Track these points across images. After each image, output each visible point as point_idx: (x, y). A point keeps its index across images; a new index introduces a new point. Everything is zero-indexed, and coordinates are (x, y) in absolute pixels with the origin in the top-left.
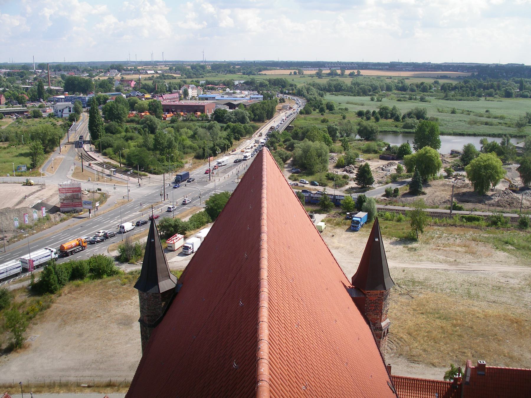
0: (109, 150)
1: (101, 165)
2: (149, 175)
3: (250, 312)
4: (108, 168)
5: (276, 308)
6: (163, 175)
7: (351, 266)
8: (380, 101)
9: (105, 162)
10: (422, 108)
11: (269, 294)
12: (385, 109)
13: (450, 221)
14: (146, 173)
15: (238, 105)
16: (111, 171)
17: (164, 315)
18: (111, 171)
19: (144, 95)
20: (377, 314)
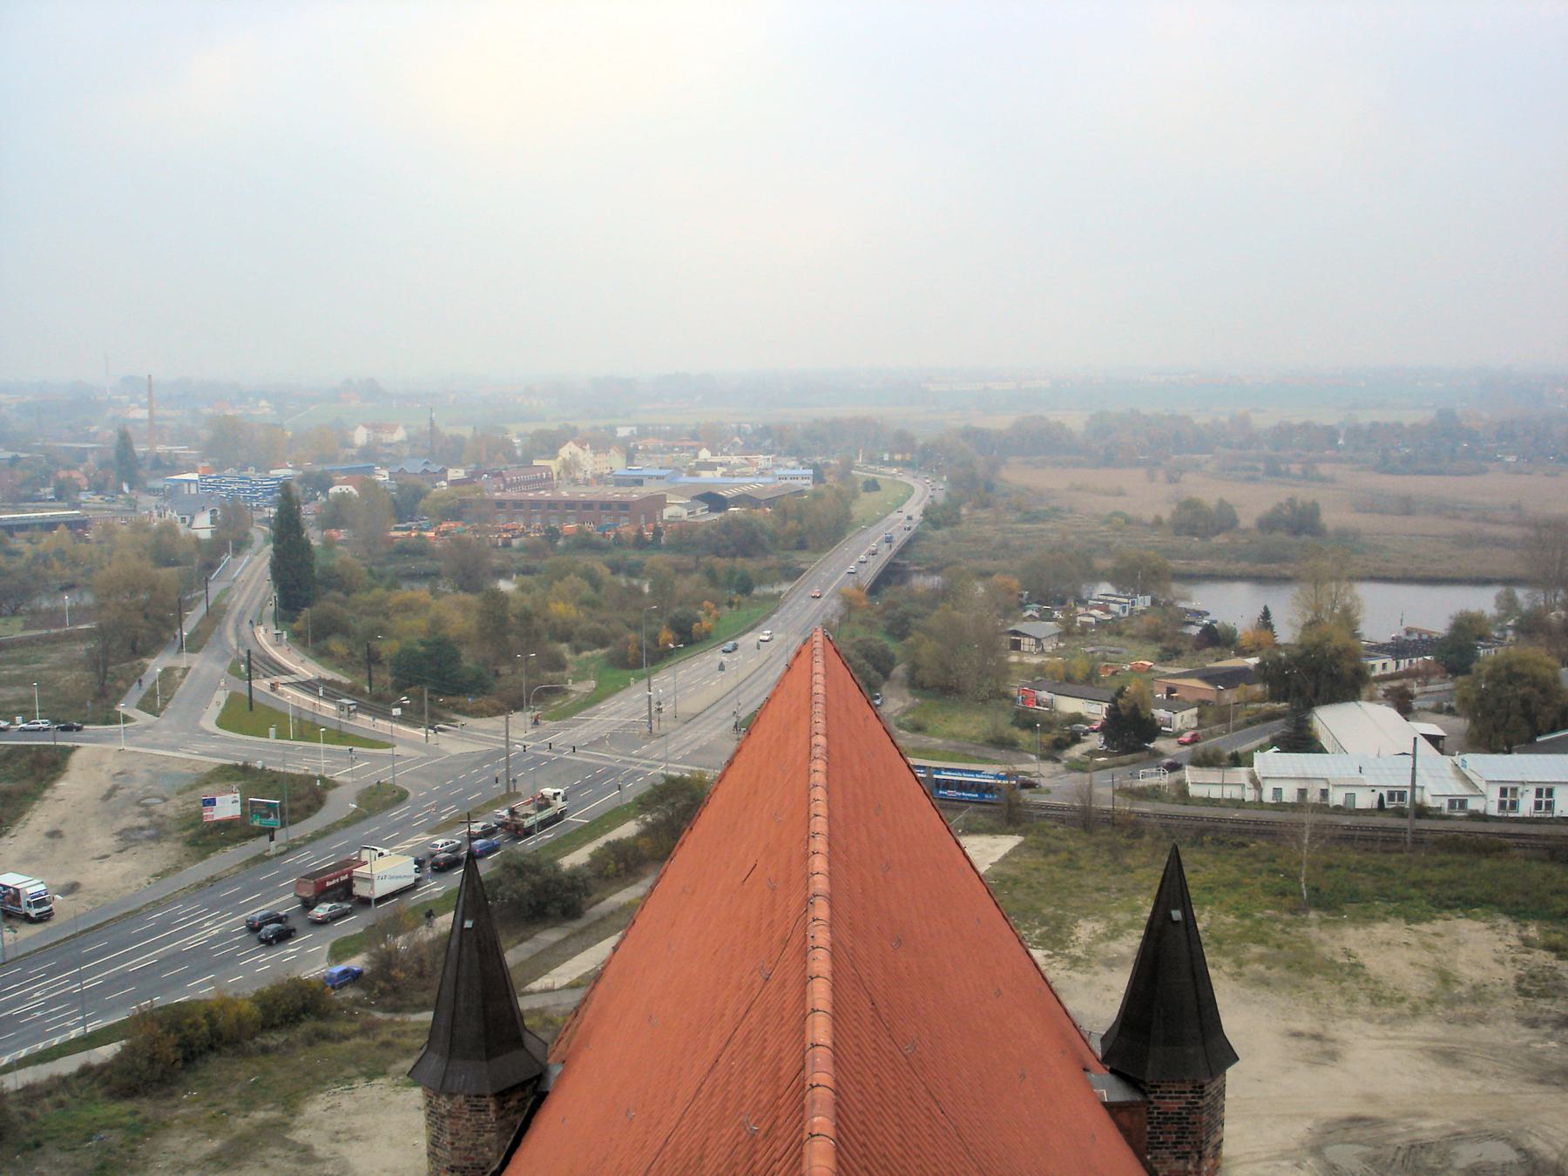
0: (336, 645)
1: (308, 686)
2: (464, 720)
3: (777, 1155)
4: (329, 697)
5: (862, 1139)
6: (503, 718)
7: (1098, 997)
8: (1176, 481)
9: (321, 681)
10: (1431, 414)
11: (837, 1093)
12: (1191, 505)
13: (1397, 847)
14: (1124, 805)
15: (738, 500)
16: (342, 707)
17: (505, 1163)
18: (342, 707)
19: (444, 471)
20: (1185, 1156)
